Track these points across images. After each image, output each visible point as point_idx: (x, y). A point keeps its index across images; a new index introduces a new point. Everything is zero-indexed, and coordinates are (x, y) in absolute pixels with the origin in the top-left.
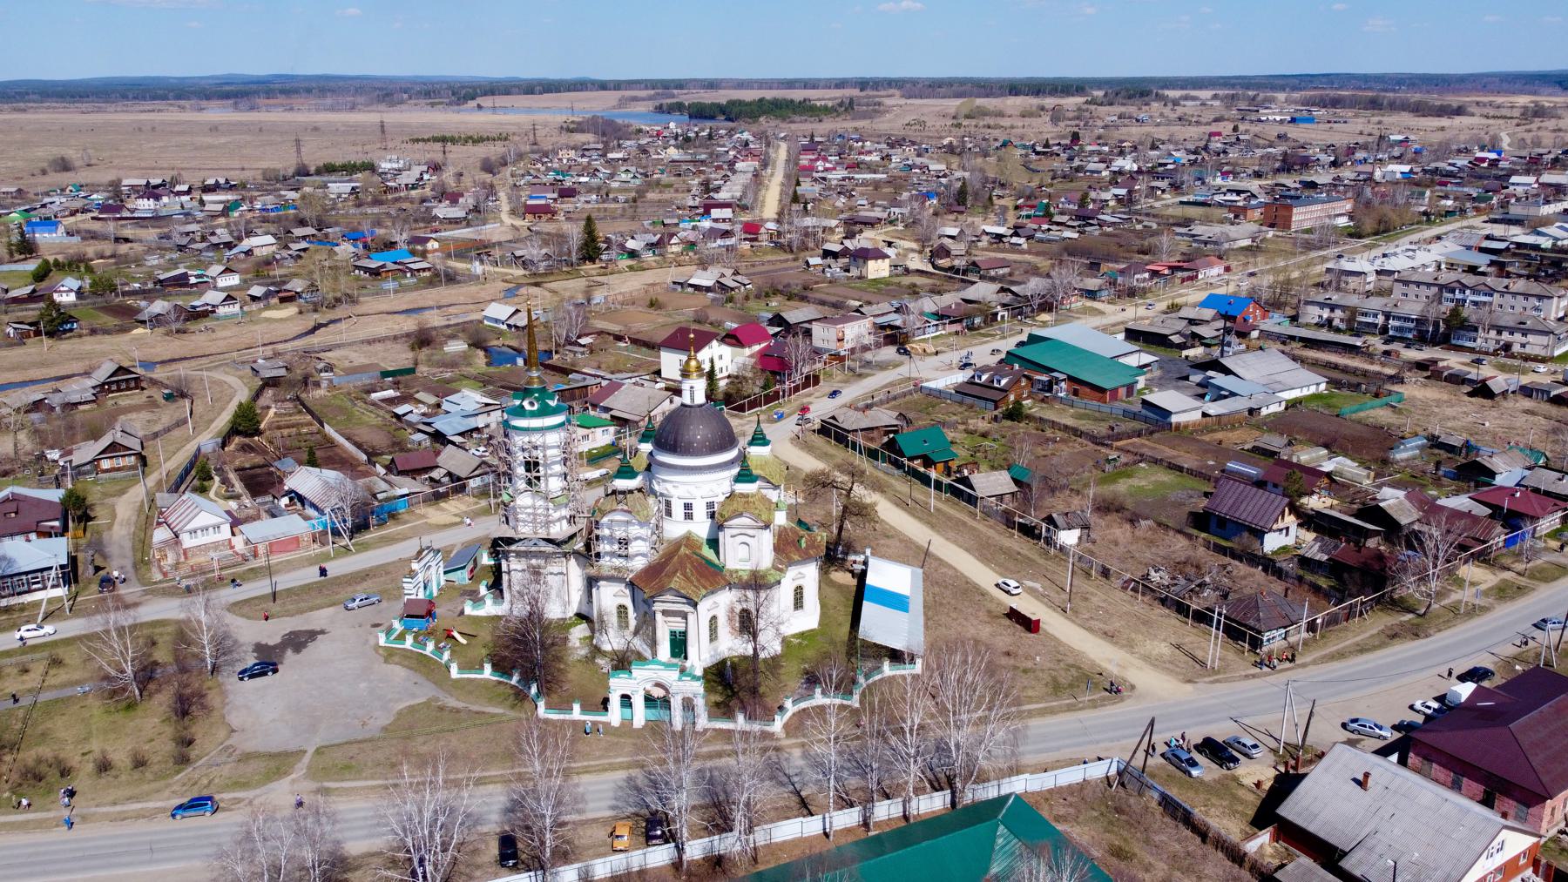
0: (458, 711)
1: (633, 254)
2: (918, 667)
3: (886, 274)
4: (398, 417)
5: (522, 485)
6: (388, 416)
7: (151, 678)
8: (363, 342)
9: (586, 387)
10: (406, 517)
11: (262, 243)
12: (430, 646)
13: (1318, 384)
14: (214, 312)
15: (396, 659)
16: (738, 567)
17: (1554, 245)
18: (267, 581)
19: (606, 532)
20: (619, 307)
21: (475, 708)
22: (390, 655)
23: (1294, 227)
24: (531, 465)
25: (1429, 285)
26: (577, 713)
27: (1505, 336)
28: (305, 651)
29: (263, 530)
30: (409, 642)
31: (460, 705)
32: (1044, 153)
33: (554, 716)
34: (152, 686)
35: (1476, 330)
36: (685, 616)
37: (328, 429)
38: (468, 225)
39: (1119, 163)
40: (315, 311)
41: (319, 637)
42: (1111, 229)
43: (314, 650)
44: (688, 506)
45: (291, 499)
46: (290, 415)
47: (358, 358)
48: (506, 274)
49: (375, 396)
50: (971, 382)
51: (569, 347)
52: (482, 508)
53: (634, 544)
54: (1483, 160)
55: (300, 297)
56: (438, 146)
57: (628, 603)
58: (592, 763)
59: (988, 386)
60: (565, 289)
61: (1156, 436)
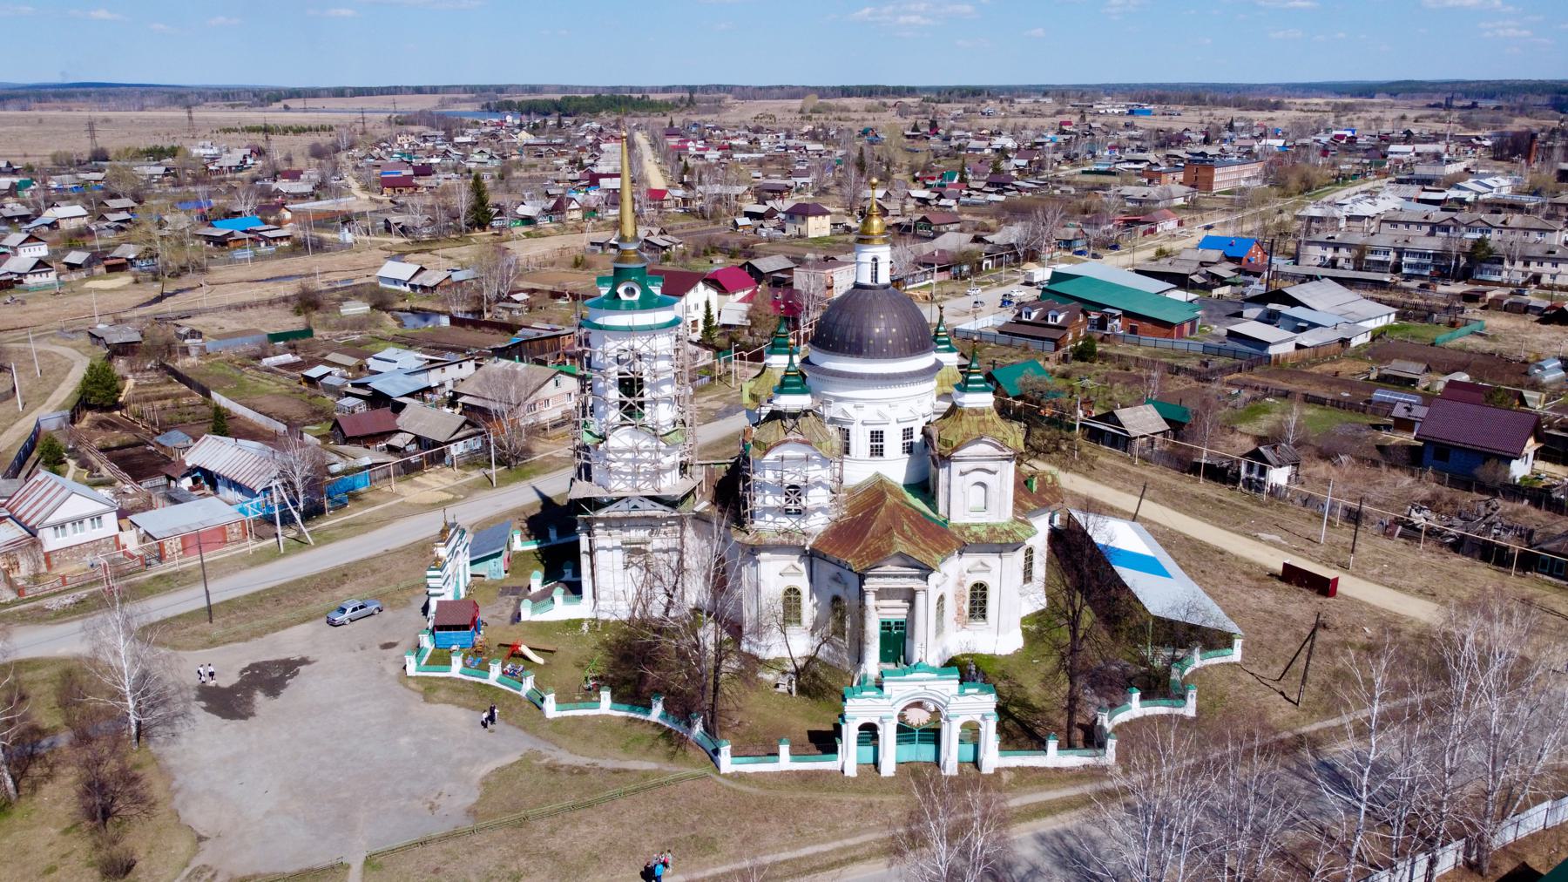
0: (582, 772)
1: (528, 221)
2: (1236, 654)
3: (827, 232)
4: (311, 381)
5: (615, 415)
6: (294, 384)
7: (32, 757)
8: (229, 308)
10: (370, 496)
11: (70, 214)
12: (495, 671)
13: (1389, 315)
14: (20, 282)
15: (442, 694)
16: (969, 520)
17: (1477, 198)
18: (200, 589)
19: (769, 476)
20: (537, 268)
21: (609, 764)
22: (429, 689)
23: (1216, 188)
24: (629, 385)
25: (1419, 224)
26: (785, 761)
27: (1534, 267)
28: (284, 692)
29: (165, 520)
30: (456, 668)
31: (581, 761)
32: (914, 137)
33: (750, 767)
34: (36, 771)
35: (1501, 261)
36: (910, 596)
37: (218, 398)
38: (318, 198)
39: (999, 142)
40: (156, 280)
41: (302, 669)
42: (1029, 194)
43: (300, 688)
44: (877, 436)
45: (195, 481)
46: (158, 385)
47: (230, 324)
48: (383, 242)
49: (265, 362)
50: (1018, 321)
51: (501, 304)
52: (476, 481)
53: (811, 493)
54: (1342, 137)
55: (133, 265)
56: (261, 136)
57: (803, 584)
58: (850, 842)
59: (1041, 323)
60: (460, 255)
61: (1256, 370)
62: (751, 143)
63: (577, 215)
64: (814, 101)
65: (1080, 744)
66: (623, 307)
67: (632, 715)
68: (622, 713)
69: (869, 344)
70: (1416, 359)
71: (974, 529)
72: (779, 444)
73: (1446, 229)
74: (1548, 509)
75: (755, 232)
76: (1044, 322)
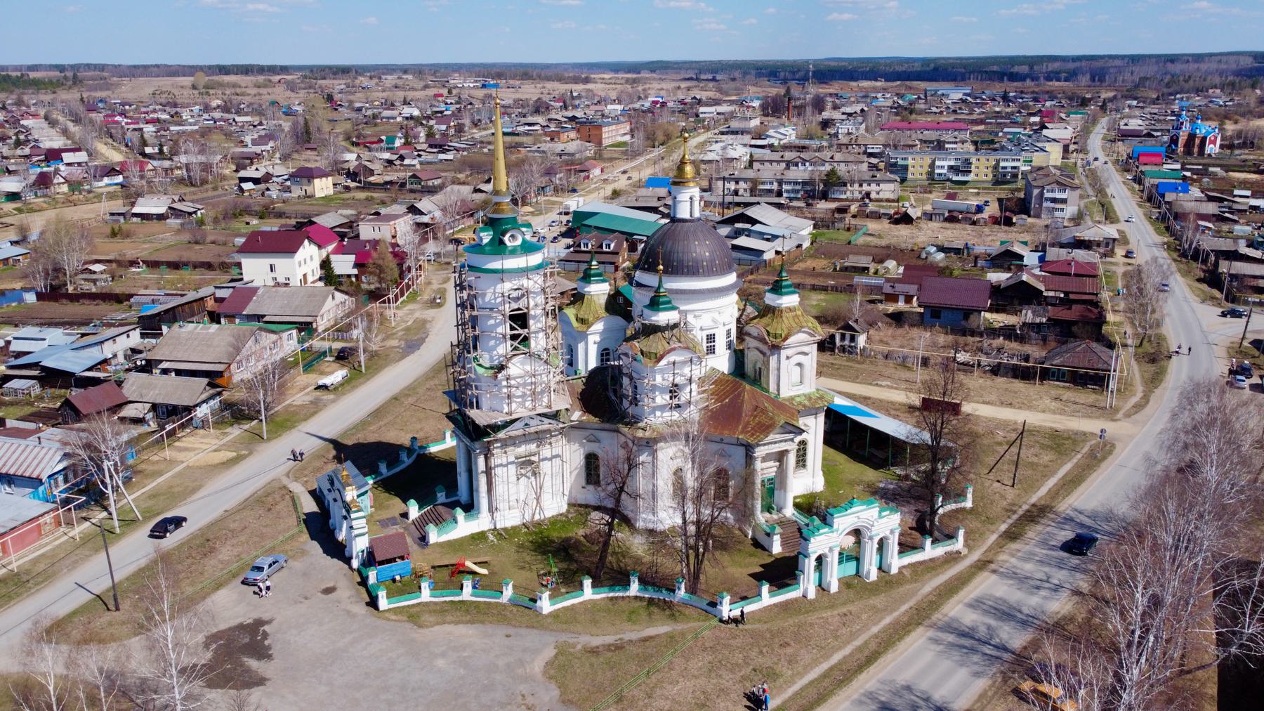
3: (330, 191)
5: (503, 349)
9: (202, 299)
21: (634, 636)
27: (865, 188)
35: (845, 185)
42: (465, 153)
62: (172, 116)
63: (65, 188)
64: (203, 79)
65: (903, 539)
66: (507, 252)
67: (611, 595)
68: (603, 594)
69: (703, 266)
70: (866, 254)
71: (798, 399)
72: (669, 352)
73: (797, 165)
74: (1016, 341)
75: (263, 194)
76: (599, 250)
